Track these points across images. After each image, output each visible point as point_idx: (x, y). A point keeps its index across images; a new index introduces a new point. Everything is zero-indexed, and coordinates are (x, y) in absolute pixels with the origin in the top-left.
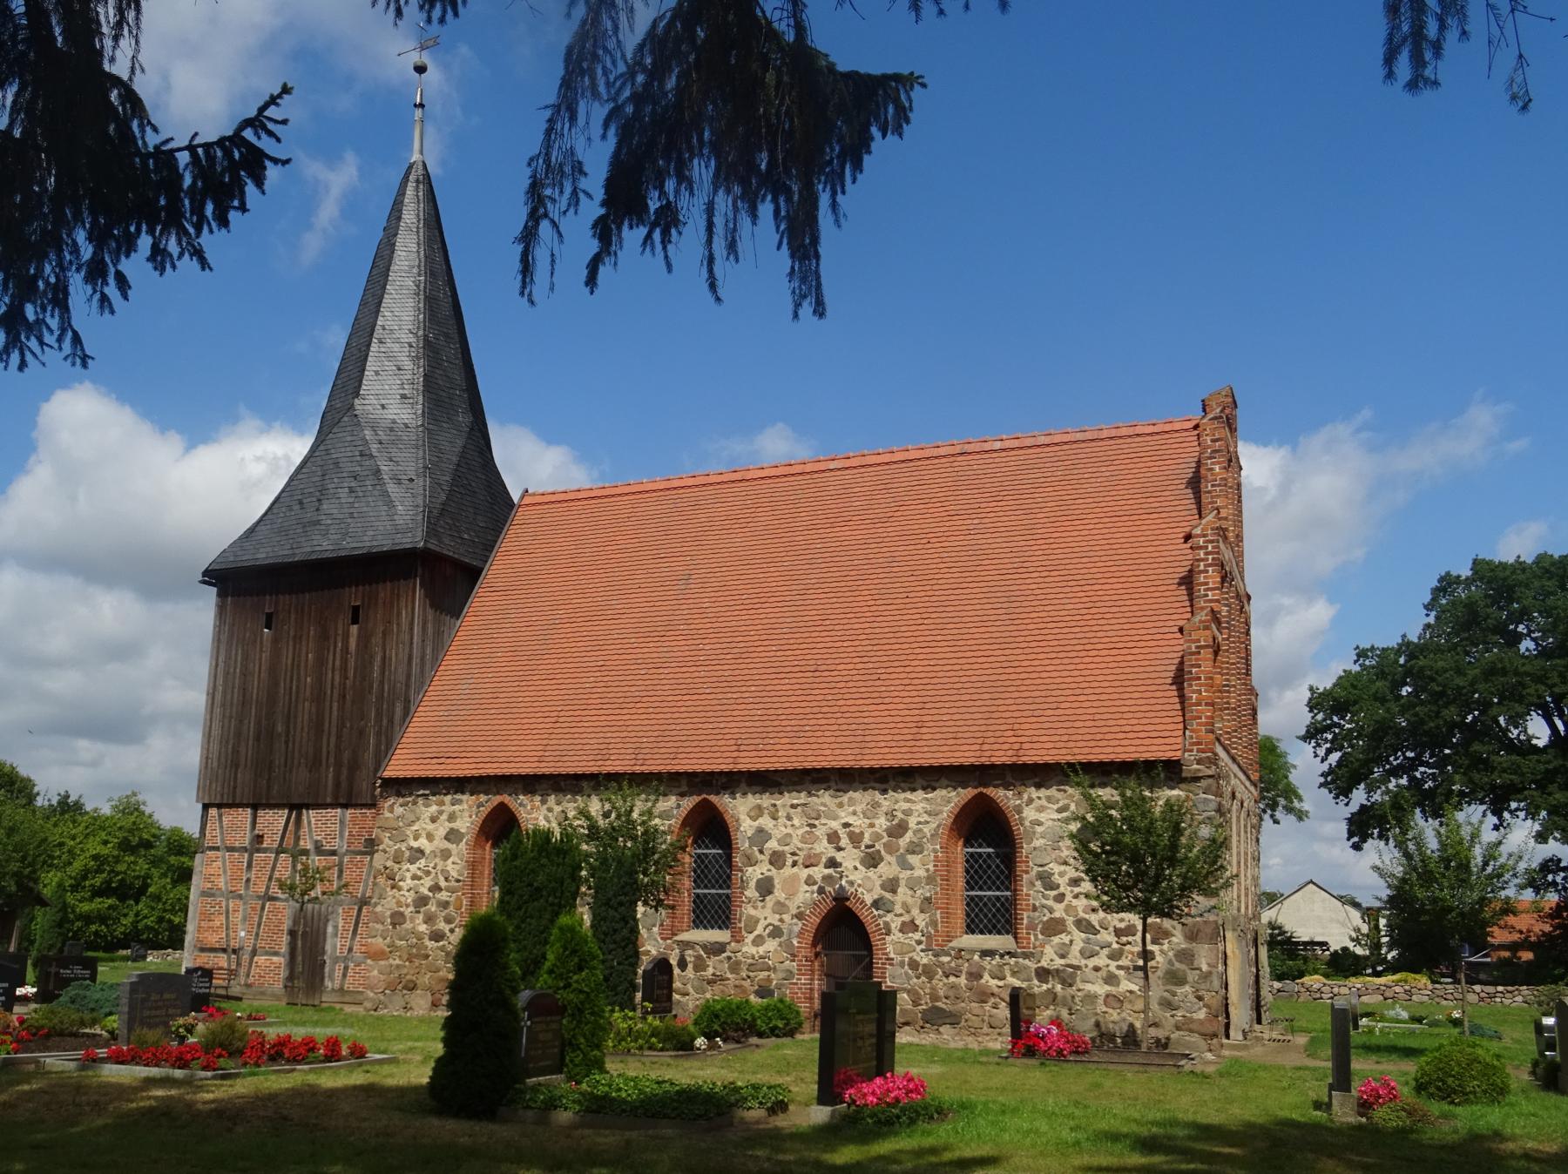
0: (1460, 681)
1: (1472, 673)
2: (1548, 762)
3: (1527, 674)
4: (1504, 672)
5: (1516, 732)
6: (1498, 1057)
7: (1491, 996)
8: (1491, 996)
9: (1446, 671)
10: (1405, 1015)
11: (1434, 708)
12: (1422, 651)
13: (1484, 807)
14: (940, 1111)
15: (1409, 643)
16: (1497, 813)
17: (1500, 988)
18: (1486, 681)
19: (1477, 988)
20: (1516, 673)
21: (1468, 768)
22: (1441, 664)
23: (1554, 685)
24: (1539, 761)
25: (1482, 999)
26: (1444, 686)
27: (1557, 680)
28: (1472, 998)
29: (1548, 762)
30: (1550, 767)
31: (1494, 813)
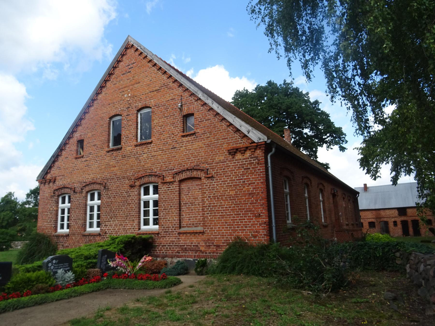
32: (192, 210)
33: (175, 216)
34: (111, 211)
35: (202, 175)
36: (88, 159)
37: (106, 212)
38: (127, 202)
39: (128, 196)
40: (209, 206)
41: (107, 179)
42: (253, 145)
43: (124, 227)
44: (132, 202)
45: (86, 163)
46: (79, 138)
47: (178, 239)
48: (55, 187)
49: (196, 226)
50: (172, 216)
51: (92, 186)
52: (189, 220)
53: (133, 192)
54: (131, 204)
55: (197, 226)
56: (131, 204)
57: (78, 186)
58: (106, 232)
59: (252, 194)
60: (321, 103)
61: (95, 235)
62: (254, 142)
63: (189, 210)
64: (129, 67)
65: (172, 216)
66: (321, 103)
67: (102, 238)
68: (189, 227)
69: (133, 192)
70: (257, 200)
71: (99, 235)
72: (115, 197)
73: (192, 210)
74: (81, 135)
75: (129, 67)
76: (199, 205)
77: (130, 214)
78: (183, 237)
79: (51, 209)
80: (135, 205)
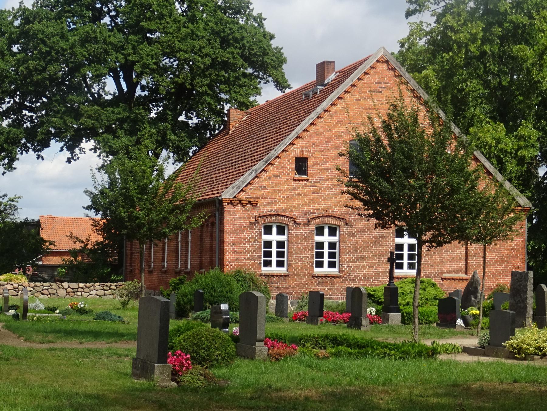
0: (63, 44)
1: (73, 39)
2: (119, 113)
3: (111, 43)
4: (96, 41)
5: (97, 88)
6: (374, 291)
7: (75, 291)
8: (75, 291)
9: (54, 36)
10: (42, 307)
11: (43, 63)
12: (35, 17)
13: (62, 144)
14: (17, 357)
15: (25, 10)
16: (71, 149)
17: (81, 285)
18: (83, 46)
19: (66, 285)
20: (105, 42)
21: (64, 113)
22: (50, 29)
23: (129, 55)
24: (113, 112)
25: (68, 293)
26: (52, 48)
27: (131, 51)
28: (62, 292)
29: (119, 113)
30: (120, 116)
31: (68, 149)
32: (454, 258)
33: (438, 262)
34: (357, 251)
35: (342, 223)
36: (316, 184)
37: (350, 251)
38: (379, 243)
39: (380, 237)
40: (475, 256)
41: (350, 214)
42: (519, 208)
43: (375, 269)
44: (386, 243)
45: (313, 190)
46: (300, 155)
47: (442, 284)
48: (257, 214)
49: (456, 273)
50: (435, 262)
51: (326, 219)
52: (450, 267)
53: (387, 233)
54: (385, 245)
55: (458, 273)
56: (385, 245)
57: (300, 216)
58: (349, 274)
59: (513, 249)
60: (4, 173)
61: (333, 277)
62: (520, 206)
63: (450, 258)
64: (380, 85)
65: (435, 262)
66: (4, 173)
67: (343, 280)
68: (449, 273)
69: (387, 233)
70: (517, 255)
71: (285, 276)
72: (362, 236)
73: (454, 258)
74: (302, 151)
75: (380, 85)
76: (461, 253)
77: (383, 256)
78: (447, 283)
79: (251, 240)
80: (390, 248)
